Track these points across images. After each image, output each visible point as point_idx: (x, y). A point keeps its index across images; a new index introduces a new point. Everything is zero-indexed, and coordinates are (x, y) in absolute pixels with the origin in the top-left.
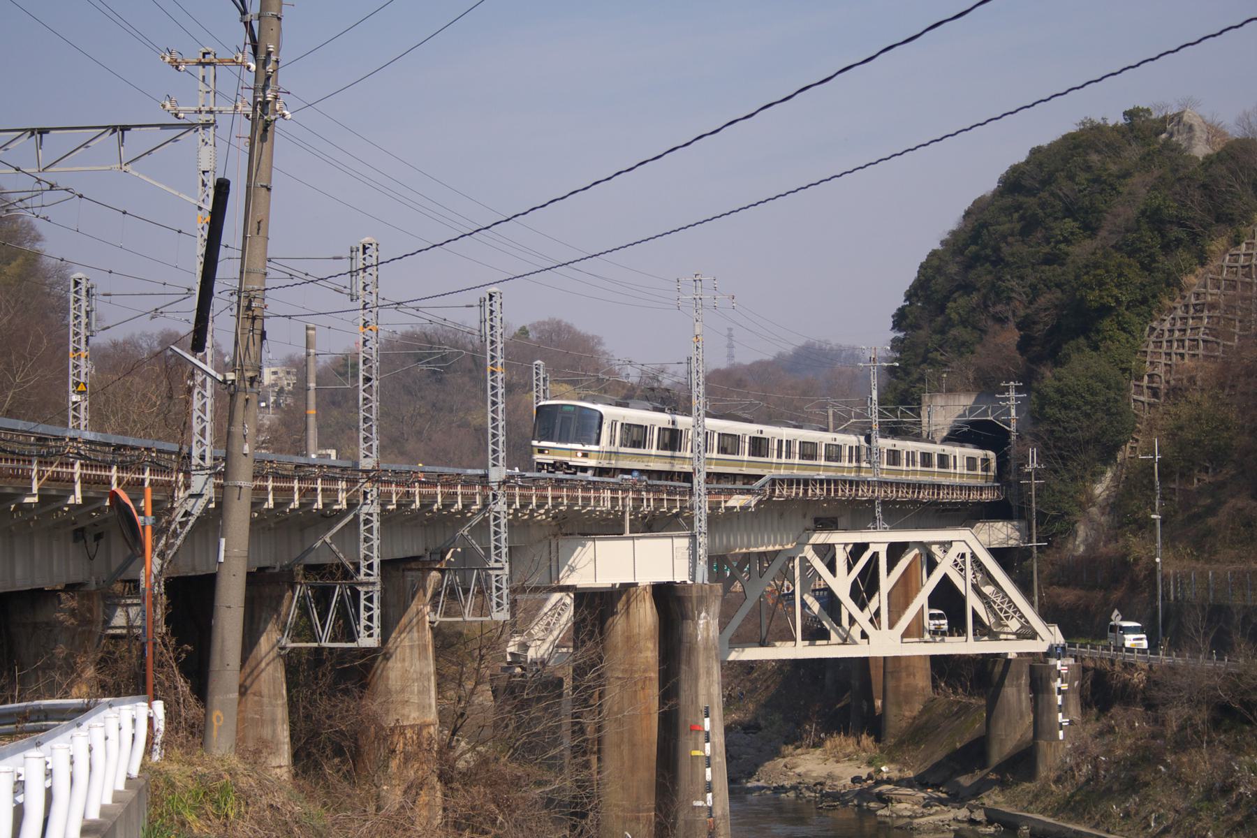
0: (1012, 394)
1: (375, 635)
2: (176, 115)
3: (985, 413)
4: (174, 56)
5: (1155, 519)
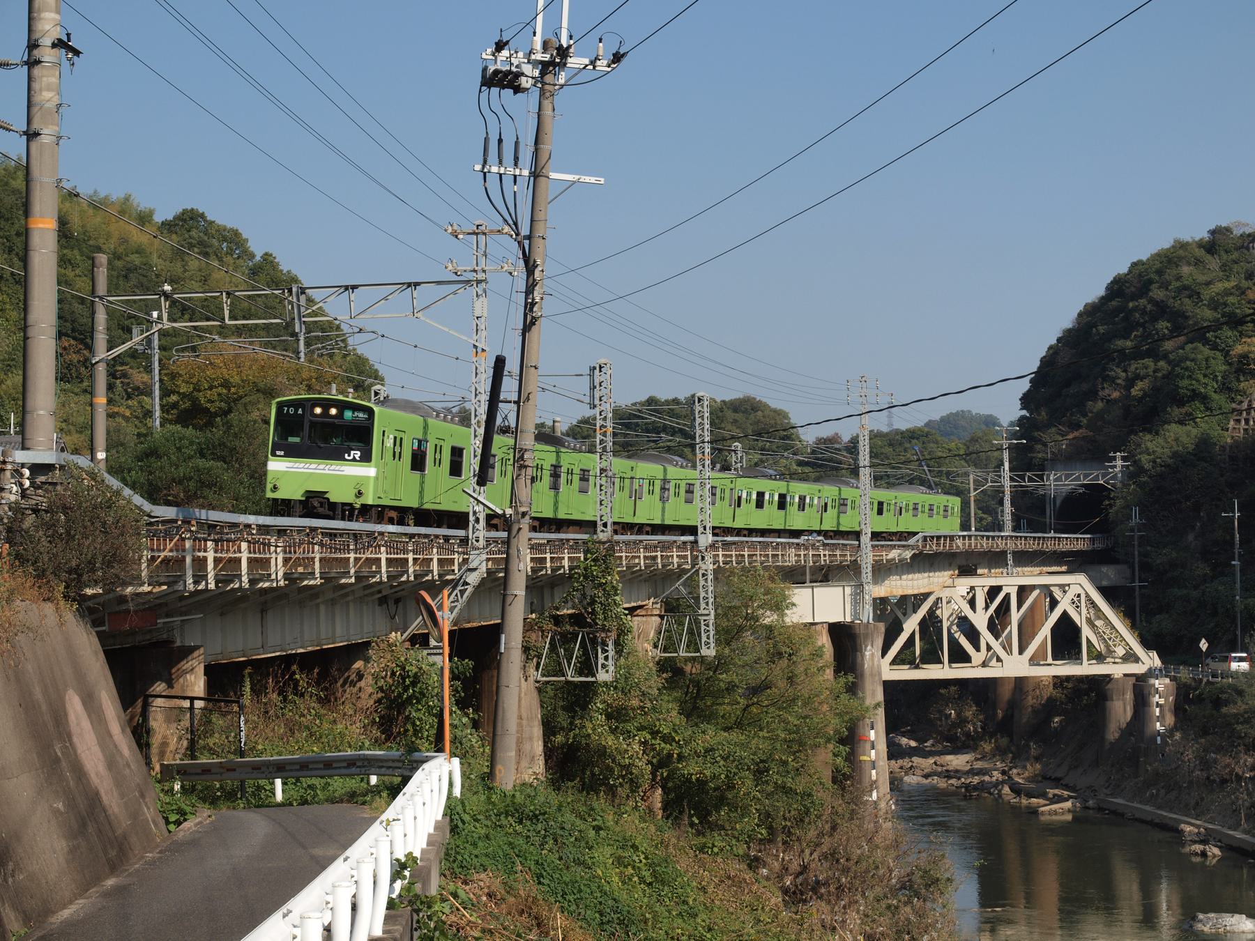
2: (456, 273)
3: (1097, 478)
4: (456, 227)
5: (1234, 565)
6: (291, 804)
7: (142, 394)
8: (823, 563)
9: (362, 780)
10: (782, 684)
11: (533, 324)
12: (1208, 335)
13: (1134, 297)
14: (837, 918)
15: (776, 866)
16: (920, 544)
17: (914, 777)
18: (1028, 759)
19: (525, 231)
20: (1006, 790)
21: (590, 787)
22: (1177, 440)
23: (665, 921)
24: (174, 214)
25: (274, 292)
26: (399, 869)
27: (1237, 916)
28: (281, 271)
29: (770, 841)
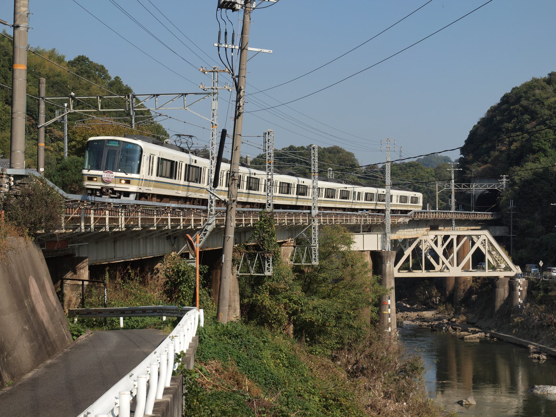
0: (505, 180)
1: (271, 271)
2: (204, 90)
3: (494, 186)
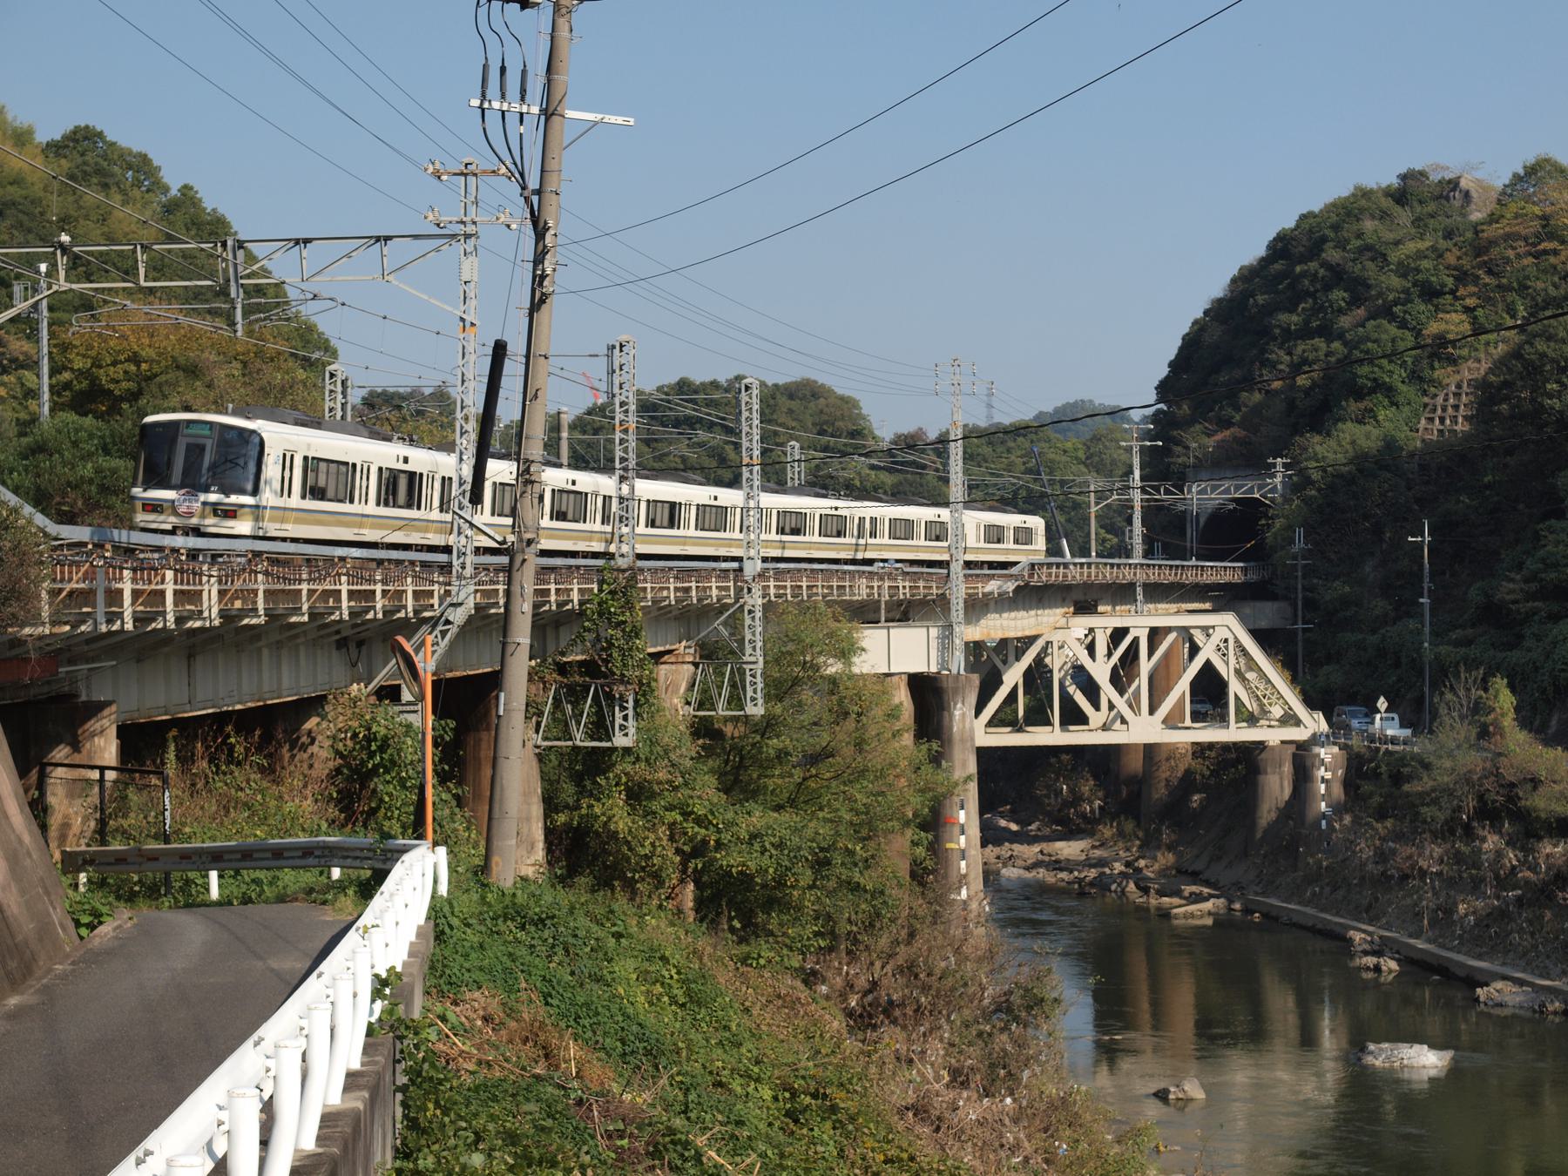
1: (630, 735)
2: (438, 225)
3: (1251, 490)
4: (438, 166)
6: (230, 903)
7: (22, 367)
8: (902, 597)
9: (321, 873)
10: (848, 751)
11: (542, 301)
12: (1394, 309)
13: (1303, 259)
14: (914, 1047)
15: (839, 981)
16: (1026, 574)
17: (1015, 870)
18: (1159, 848)
19: (533, 183)
20: (1131, 886)
21: (604, 882)
22: (1353, 442)
23: (702, 1051)
24: (63, 132)
25: (203, 246)
26: (380, 985)
27: (1417, 1047)
28: (205, 209)
29: (831, 949)
